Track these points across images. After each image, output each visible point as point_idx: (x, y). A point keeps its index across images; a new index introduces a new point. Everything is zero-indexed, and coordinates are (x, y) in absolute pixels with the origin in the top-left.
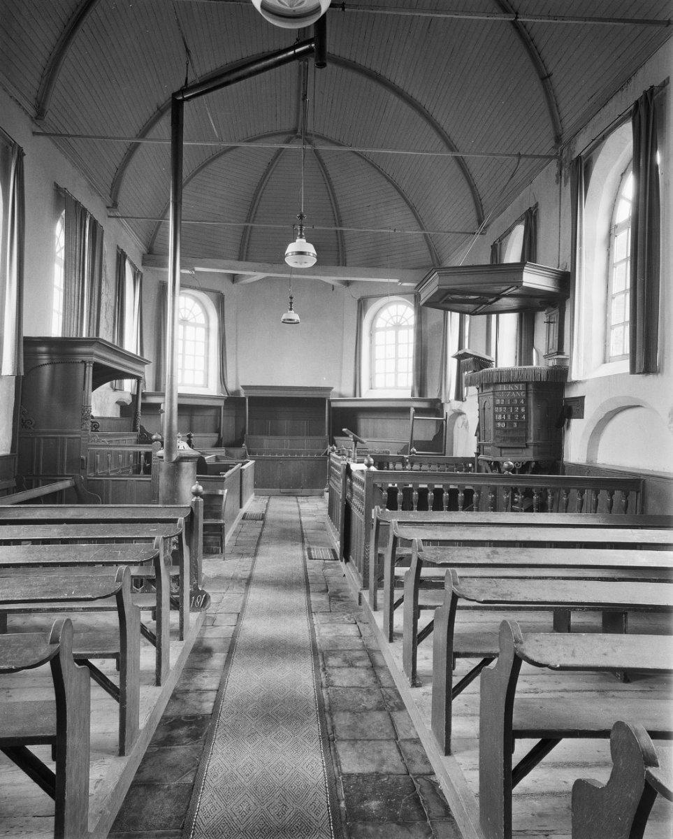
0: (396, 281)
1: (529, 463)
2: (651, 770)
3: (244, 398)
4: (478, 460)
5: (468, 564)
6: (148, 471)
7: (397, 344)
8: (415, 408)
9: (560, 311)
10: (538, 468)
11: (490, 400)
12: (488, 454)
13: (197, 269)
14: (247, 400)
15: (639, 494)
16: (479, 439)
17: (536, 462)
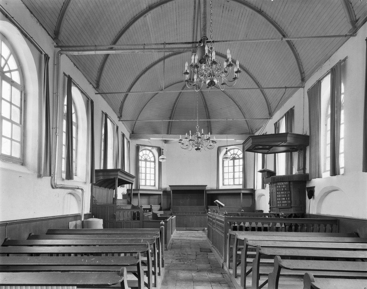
0: (233, 139)
1: (292, 214)
2: (313, 283)
3: (170, 191)
4: (270, 214)
5: (266, 274)
6: (138, 219)
7: (234, 166)
8: (242, 193)
9: (304, 151)
10: (296, 216)
11: (274, 189)
12: (274, 211)
13: (151, 139)
14: (171, 191)
15: (337, 226)
16: (270, 205)
17: (295, 214)
